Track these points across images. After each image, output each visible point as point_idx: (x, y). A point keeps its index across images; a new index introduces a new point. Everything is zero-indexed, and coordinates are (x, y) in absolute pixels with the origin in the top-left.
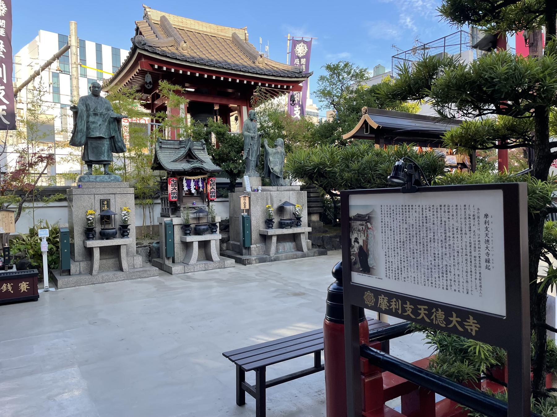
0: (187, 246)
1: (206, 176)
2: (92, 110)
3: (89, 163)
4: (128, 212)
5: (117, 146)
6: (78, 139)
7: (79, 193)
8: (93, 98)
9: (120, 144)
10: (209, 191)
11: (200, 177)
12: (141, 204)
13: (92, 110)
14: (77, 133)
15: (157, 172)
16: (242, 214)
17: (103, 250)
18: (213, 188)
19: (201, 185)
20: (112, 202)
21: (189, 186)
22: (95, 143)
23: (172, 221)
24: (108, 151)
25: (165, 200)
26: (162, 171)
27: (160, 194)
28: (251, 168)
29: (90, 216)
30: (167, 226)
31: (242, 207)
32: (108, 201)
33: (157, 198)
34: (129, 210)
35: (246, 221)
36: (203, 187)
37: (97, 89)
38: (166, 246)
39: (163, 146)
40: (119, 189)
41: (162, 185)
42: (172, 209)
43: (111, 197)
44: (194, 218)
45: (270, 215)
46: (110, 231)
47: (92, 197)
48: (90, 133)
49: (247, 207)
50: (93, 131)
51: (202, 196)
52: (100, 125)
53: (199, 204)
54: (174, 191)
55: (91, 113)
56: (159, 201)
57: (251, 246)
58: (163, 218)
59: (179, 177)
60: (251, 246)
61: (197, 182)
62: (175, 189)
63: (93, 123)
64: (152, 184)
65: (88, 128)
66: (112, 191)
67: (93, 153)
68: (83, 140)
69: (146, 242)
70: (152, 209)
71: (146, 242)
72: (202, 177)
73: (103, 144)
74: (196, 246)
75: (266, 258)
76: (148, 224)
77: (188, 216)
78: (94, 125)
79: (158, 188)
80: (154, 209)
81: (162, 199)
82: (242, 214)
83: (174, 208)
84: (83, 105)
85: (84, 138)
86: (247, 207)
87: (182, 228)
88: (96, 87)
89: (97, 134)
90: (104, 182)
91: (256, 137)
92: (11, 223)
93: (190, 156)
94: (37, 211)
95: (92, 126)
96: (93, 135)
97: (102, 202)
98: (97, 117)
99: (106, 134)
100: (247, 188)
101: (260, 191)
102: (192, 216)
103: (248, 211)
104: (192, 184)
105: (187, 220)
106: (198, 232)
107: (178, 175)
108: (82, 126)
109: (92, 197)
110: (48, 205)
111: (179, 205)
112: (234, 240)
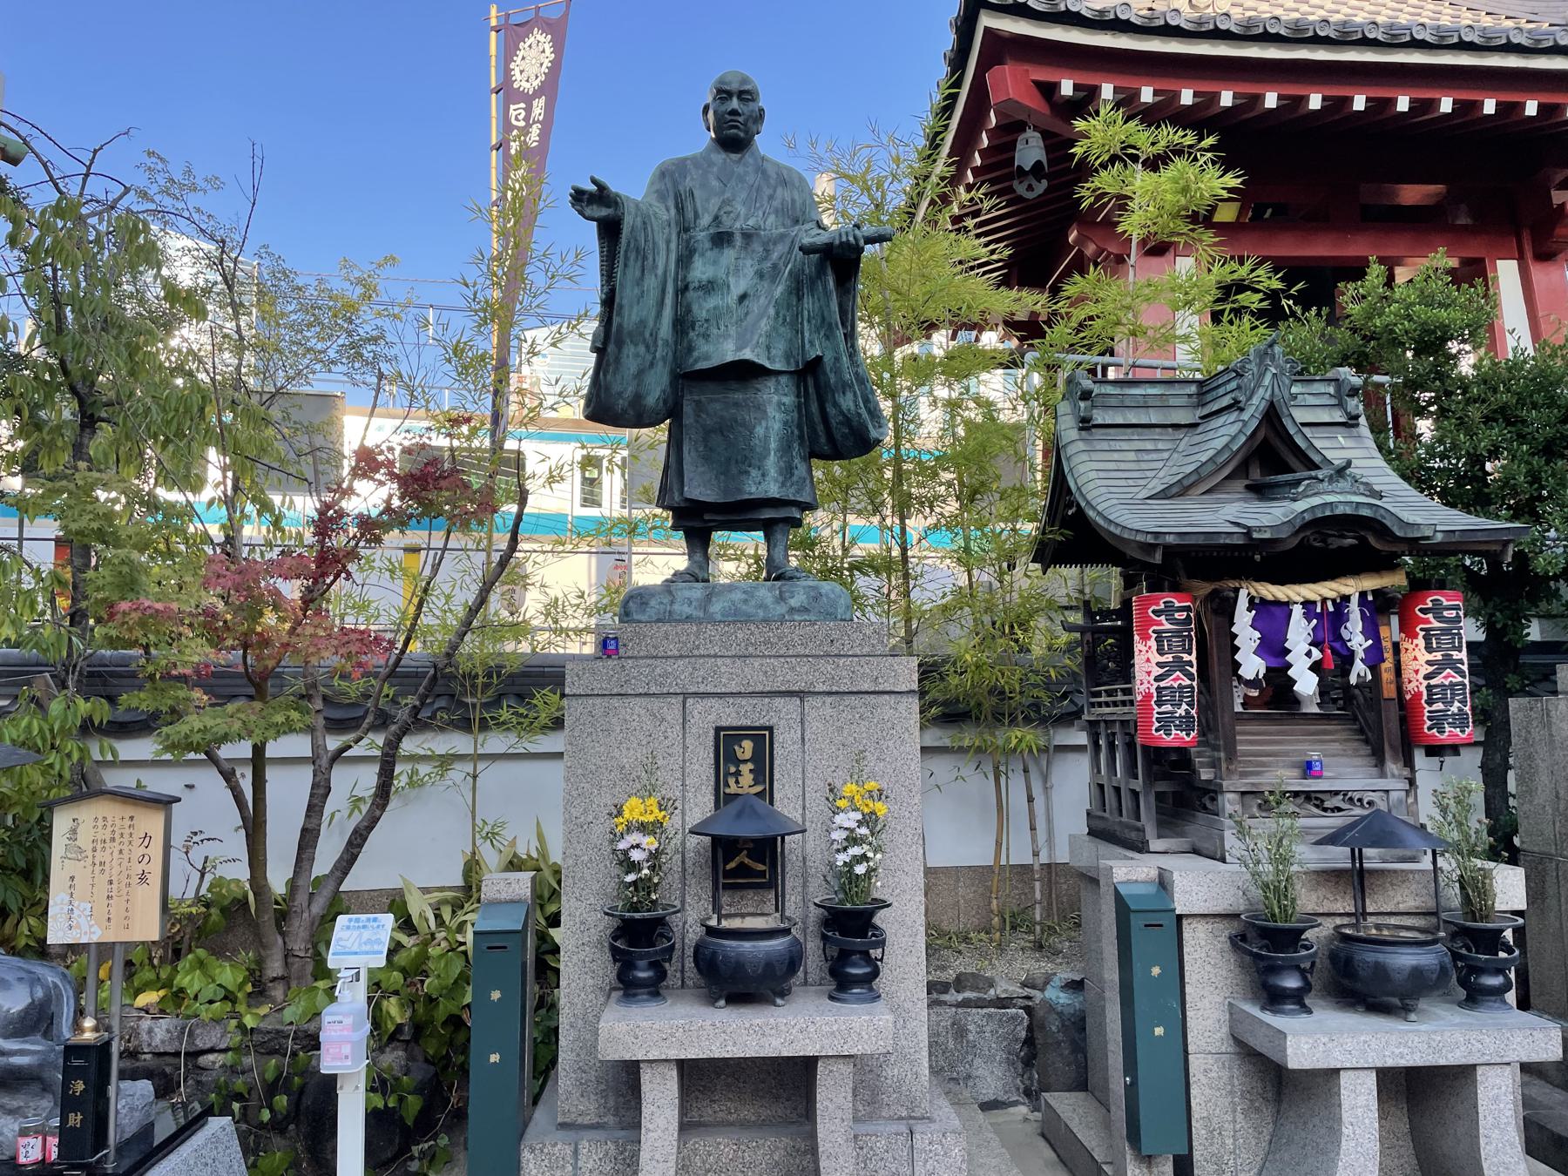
0: (1286, 1092)
1: (1394, 581)
2: (705, 220)
3: (697, 523)
4: (869, 820)
5: (838, 430)
6: (623, 386)
7: (597, 688)
8: (720, 157)
9: (847, 402)
11: (1351, 587)
12: (979, 750)
13: (705, 220)
14: (620, 344)
15: (1067, 580)
17: (698, 1077)
18: (1448, 662)
21: (1274, 648)
22: (718, 403)
23: (1163, 883)
24: (785, 448)
25: (1118, 739)
26: (1093, 572)
27: (1082, 700)
29: (635, 838)
30: (1136, 922)
32: (763, 738)
33: (1069, 719)
34: (881, 808)
36: (1374, 658)
37: (735, 103)
38: (1130, 1065)
39: (1100, 417)
40: (827, 667)
41: (1095, 643)
42: (1160, 797)
43: (782, 715)
44: (1331, 876)
46: (747, 945)
47: (672, 710)
48: (690, 349)
50: (706, 336)
51: (1380, 722)
52: (743, 298)
53: (1347, 772)
54: (1178, 680)
55: (701, 236)
56: (1082, 738)
58: (1105, 848)
59: (1204, 588)
61: (1329, 621)
62: (1180, 665)
63: (709, 287)
64: (1049, 640)
65: (683, 324)
66: (786, 677)
68: (656, 387)
69: (1009, 972)
70: (1045, 778)
71: (1009, 972)
72: (1370, 583)
73: (760, 408)
74: (1359, 1103)
76: (1019, 853)
77: (1282, 860)
78: (712, 302)
79: (1073, 663)
80: (1055, 778)
81: (1093, 727)
83: (1172, 792)
84: (662, 197)
85: (660, 385)
87: (1238, 942)
88: (729, 94)
89: (728, 351)
90: (748, 619)
92: (143, 878)
93: (1272, 457)
94: (491, 775)
95: (703, 308)
96: (707, 357)
97: (726, 740)
98: (729, 255)
99: (780, 348)
102: (1308, 856)
104: (1299, 634)
105: (1279, 891)
106: (1359, 985)
107: (1203, 570)
108: (647, 306)
109: (672, 710)
110: (533, 748)
111: (1206, 774)
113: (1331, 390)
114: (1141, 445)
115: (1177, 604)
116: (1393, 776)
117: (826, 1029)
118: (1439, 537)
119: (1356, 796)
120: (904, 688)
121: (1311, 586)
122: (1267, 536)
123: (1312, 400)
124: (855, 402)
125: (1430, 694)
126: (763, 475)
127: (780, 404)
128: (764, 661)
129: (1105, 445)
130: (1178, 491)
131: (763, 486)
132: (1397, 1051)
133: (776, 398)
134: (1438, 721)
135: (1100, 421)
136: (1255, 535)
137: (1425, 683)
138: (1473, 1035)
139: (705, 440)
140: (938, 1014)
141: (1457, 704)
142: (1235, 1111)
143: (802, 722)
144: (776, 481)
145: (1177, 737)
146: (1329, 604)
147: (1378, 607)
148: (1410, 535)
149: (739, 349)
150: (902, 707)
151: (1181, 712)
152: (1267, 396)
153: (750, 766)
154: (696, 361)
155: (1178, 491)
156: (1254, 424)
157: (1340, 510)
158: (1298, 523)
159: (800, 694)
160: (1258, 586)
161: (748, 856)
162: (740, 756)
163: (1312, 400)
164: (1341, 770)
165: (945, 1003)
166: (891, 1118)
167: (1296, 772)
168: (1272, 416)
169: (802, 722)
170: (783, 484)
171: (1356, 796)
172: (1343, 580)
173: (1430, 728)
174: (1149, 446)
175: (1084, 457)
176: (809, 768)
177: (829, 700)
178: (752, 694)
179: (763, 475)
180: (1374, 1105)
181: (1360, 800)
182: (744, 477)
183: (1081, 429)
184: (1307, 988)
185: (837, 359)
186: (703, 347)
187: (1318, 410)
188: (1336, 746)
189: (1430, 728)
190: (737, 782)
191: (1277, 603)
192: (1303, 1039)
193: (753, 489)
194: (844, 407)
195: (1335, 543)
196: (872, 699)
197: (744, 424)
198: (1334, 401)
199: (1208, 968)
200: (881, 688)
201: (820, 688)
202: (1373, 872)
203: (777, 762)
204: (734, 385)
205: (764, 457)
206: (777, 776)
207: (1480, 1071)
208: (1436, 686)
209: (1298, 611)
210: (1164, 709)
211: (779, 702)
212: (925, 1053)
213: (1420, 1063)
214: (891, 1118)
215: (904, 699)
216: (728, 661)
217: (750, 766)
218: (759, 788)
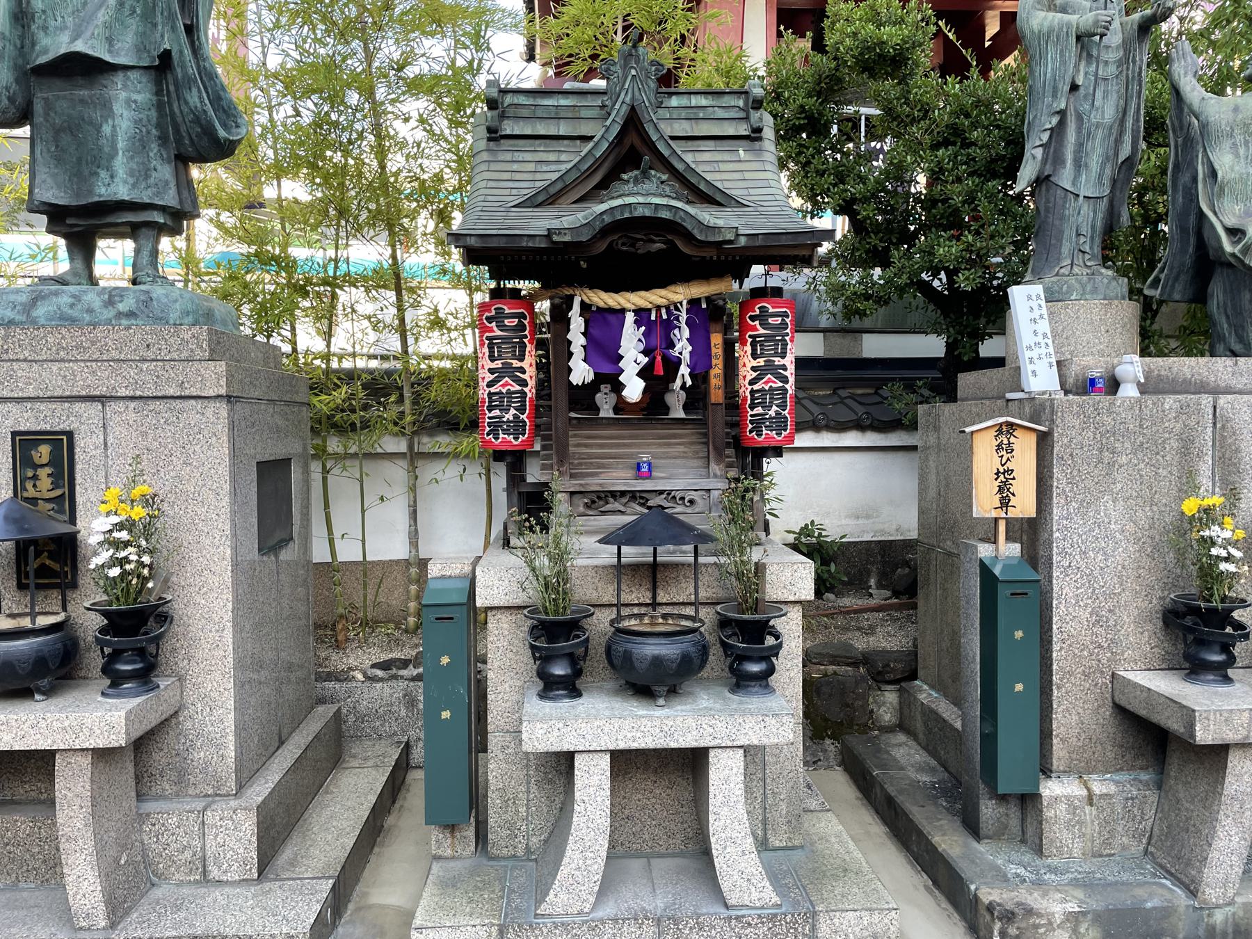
10: (745, 390)
11: (680, 294)
16: (984, 551)
19: (683, 347)
20: (87, 449)
22: (56, 99)
24: (139, 146)
28: (1066, 249)
31: (984, 503)
32: (62, 446)
35: (1018, 602)
39: (509, 128)
43: (84, 423)
45: (1209, 574)
49: (1024, 504)
57: (1050, 789)
60: (1050, 789)
61: (657, 330)
66: (85, 380)
67: (59, 160)
72: (699, 290)
73: (106, 106)
75: (1166, 912)
82: (984, 551)
86: (1024, 504)
91: (1115, 38)
96: (46, 51)
97: (24, 443)
100: (1027, 368)
101: (1129, 391)
103: (1031, 533)
112: (938, 686)
113: (741, 103)
114: (544, 157)
115: (507, 311)
116: (715, 476)
117: (57, 725)
118: (743, 241)
119: (679, 495)
120: (211, 393)
121: (643, 293)
122: (567, 238)
123: (721, 113)
124: (200, 97)
125: (753, 399)
126: (112, 177)
127: (128, 102)
128: (63, 365)
129: (508, 156)
130: (549, 198)
131: (113, 188)
132: (629, 735)
133: (123, 95)
134: (758, 424)
135: (508, 132)
136: (555, 238)
137: (750, 388)
138: (705, 721)
139: (56, 140)
140: (392, 688)
141: (775, 408)
142: (528, 783)
143: (104, 426)
144: (125, 182)
145: (505, 441)
146: (663, 311)
147: (708, 316)
148: (711, 239)
149: (73, 40)
150: (209, 412)
151: (509, 416)
152: (628, 100)
153: (48, 470)
154: (38, 56)
155: (549, 198)
156: (616, 129)
157: (639, 212)
158: (598, 226)
159: (101, 399)
160: (590, 293)
161: (50, 558)
162: (37, 461)
163: (721, 113)
164: (675, 471)
165: (402, 677)
166: (197, 796)
167: (631, 473)
168: (633, 122)
169: (104, 426)
170: (134, 186)
171: (679, 495)
172: (672, 288)
173: (751, 432)
174: (552, 157)
175: (484, 167)
176: (113, 473)
177: (132, 405)
178: (52, 399)
179: (112, 177)
180: (607, 784)
181: (683, 499)
182: (93, 179)
183: (489, 139)
184: (578, 673)
185: (181, 52)
186: (44, 41)
187: (726, 123)
188: (682, 448)
189: (751, 432)
190: (35, 486)
191: (611, 310)
192: (539, 725)
193: (103, 191)
194: (191, 104)
195: (642, 249)
196: (178, 404)
197: (91, 123)
198: (742, 115)
199: (510, 655)
200: (187, 393)
201: (123, 392)
202: (666, 566)
203: (78, 467)
204: (81, 81)
205: (113, 156)
206: (79, 479)
207: (712, 753)
208: (758, 391)
209: (630, 318)
210: (755, 412)
211: (79, 407)
212: (231, 738)
213: (651, 746)
214: (197, 796)
215: (212, 404)
216: (25, 365)
217: (48, 470)
218: (58, 492)
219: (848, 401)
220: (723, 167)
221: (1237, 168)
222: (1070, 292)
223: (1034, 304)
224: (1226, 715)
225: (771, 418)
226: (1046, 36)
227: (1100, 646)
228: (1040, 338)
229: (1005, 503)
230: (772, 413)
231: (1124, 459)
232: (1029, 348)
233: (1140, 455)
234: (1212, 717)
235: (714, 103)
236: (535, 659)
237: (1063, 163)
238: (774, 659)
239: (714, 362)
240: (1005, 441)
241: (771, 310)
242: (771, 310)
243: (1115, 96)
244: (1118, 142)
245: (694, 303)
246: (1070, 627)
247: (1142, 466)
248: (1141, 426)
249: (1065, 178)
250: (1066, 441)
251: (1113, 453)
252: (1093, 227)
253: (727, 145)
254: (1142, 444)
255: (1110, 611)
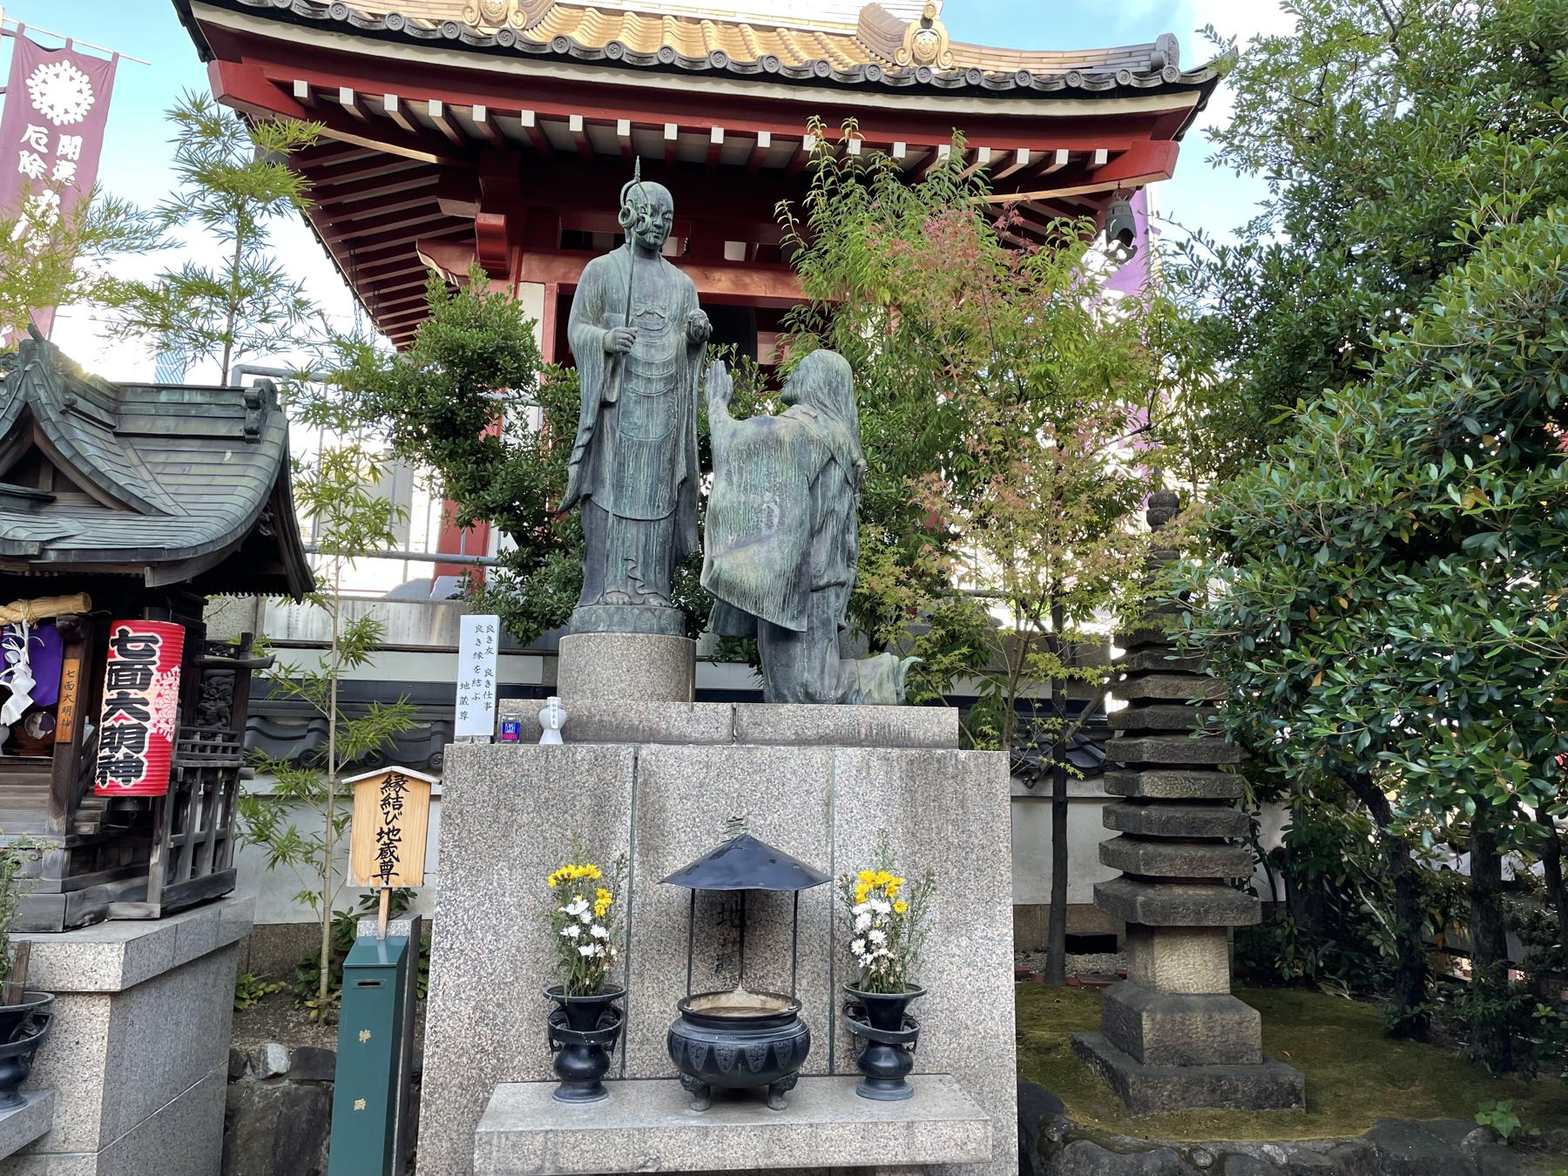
101: (551, 738)
123: (217, 412)
187: (221, 422)
219: (1090, 748)
220: (194, 470)
221: (728, 496)
222: (597, 623)
223: (483, 637)
224: (513, 1138)
225: (118, 762)
226: (587, 346)
227: (483, 1051)
228: (481, 676)
229: (386, 870)
230: (120, 755)
231: (525, 818)
232: (466, 686)
233: (544, 814)
234: (495, 1142)
235: (211, 400)
236: (554, 1049)
237: (602, 482)
238: (609, 1053)
239: (65, 692)
240: (393, 795)
241: (132, 634)
242: (132, 634)
243: (662, 415)
244: (673, 462)
245: (43, 624)
246: (447, 1026)
247: (546, 826)
248: (547, 780)
249: (605, 499)
250: (455, 795)
251: (512, 811)
252: (645, 552)
253: (214, 446)
254: (547, 800)
255: (499, 1005)
